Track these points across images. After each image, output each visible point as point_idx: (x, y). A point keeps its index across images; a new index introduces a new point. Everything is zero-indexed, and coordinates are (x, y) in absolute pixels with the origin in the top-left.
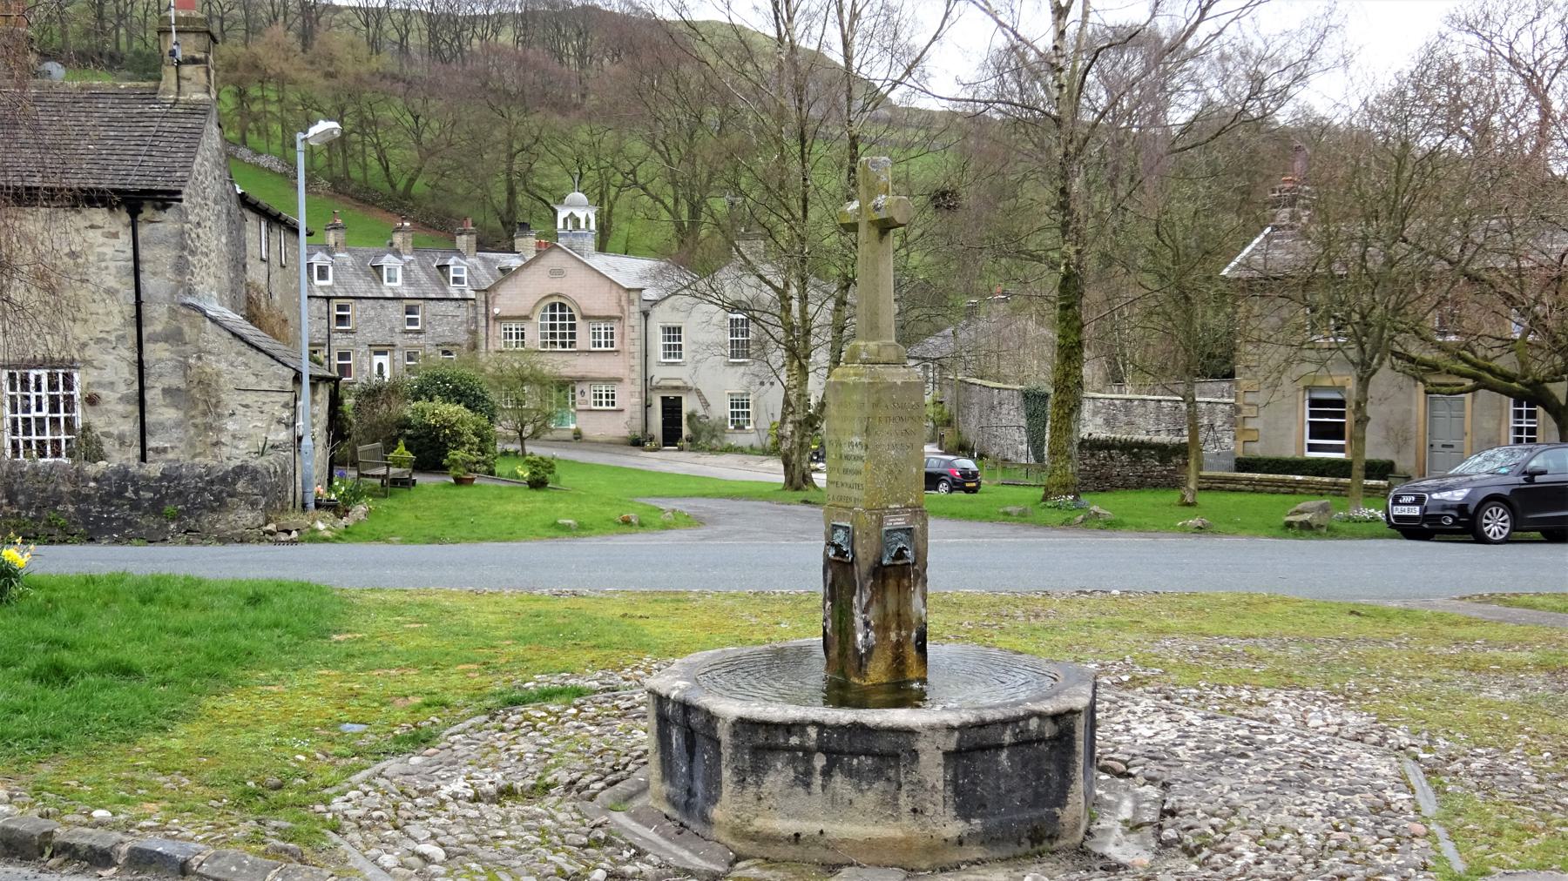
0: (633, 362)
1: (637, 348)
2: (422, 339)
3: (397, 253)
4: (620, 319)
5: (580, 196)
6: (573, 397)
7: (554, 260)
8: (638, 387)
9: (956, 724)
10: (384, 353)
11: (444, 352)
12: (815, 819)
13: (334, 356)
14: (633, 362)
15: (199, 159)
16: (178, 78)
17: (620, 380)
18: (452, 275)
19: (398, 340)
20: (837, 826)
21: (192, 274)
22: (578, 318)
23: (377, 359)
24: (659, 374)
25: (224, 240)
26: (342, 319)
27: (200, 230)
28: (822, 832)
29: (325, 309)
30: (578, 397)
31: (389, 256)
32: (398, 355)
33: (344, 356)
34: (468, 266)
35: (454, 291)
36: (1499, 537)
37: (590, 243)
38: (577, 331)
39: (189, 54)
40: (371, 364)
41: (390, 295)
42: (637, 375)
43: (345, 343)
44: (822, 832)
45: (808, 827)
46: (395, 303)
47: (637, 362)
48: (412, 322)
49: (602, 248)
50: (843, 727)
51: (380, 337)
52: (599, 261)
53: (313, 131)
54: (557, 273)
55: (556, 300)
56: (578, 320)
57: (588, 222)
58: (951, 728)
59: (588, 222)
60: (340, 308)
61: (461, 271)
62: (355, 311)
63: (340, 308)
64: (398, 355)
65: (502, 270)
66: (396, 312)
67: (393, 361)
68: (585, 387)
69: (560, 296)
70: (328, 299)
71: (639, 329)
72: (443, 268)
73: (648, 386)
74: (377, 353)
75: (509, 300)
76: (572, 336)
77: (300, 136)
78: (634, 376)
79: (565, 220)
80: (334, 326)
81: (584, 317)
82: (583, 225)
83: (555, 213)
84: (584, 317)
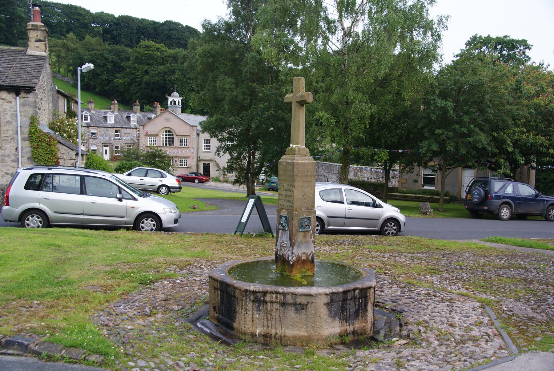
7: (167, 115)
8: (195, 160)
10: (107, 146)
15: (42, 76)
17: (189, 157)
23: (105, 148)
25: (51, 105)
30: (174, 162)
37: (179, 110)
38: (175, 140)
42: (195, 155)
46: (111, 129)
48: (118, 136)
49: (183, 111)
55: (168, 129)
57: (179, 102)
58: (327, 294)
59: (179, 102)
66: (112, 132)
69: (169, 128)
73: (199, 161)
74: (105, 146)
76: (173, 141)
77: (79, 68)
78: (193, 155)
81: (177, 135)
82: (177, 103)
84: (177, 135)
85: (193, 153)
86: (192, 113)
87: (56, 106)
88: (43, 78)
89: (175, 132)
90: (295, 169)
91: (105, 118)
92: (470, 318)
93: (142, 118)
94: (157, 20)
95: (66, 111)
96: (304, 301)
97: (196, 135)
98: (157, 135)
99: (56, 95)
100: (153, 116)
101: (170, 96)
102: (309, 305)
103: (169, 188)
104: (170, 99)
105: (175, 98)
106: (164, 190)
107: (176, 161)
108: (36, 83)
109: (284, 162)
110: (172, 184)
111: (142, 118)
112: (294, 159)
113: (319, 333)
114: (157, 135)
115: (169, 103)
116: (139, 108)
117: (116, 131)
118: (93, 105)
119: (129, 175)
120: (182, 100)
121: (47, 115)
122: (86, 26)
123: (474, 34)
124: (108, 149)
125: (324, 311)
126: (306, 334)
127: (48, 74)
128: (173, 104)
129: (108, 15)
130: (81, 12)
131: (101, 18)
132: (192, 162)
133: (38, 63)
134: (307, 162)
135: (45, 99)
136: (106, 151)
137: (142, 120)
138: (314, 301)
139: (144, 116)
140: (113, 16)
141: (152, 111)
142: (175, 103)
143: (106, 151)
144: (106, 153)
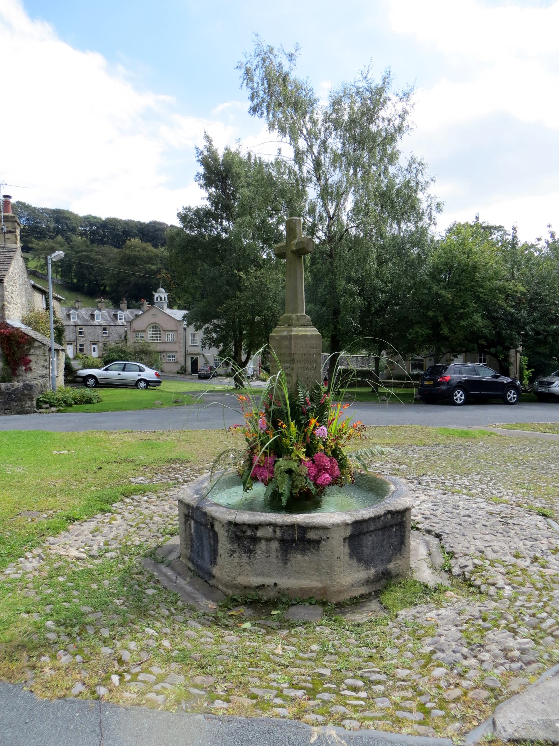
0: (181, 345)
1: (182, 341)
2: (109, 339)
3: (100, 310)
4: (176, 331)
5: (163, 290)
6: (161, 358)
7: (153, 311)
8: (183, 354)
9: (349, 522)
10: (95, 344)
11: (117, 343)
12: (270, 576)
13: (78, 345)
14: (181, 345)
15: (12, 269)
16: (5, 238)
17: (176, 352)
18: (119, 317)
19: (100, 339)
20: (284, 581)
21: (9, 311)
22: (162, 331)
23: (93, 346)
24: (190, 350)
25: (24, 299)
26: (80, 333)
27: (12, 295)
28: (275, 584)
29: (74, 329)
30: (162, 357)
31: (97, 311)
32: (100, 345)
33: (81, 345)
34: (125, 314)
35: (120, 323)
36: (513, 401)
37: (165, 305)
38: (162, 336)
39: (9, 229)
40: (91, 348)
41: (98, 324)
42: (182, 350)
43: (82, 340)
44: (275, 584)
45: (268, 581)
46: (99, 327)
47: (182, 345)
48: (106, 333)
49: (170, 307)
50: (287, 526)
51: (94, 338)
52: (169, 312)
53: (53, 255)
54: (154, 316)
55: (154, 325)
56: (162, 332)
57: (165, 298)
58: (347, 525)
59: (165, 298)
60: (80, 329)
61: (122, 316)
62: (85, 330)
63: (80, 329)
64: (100, 345)
65: (136, 315)
66: (99, 330)
67: (99, 347)
68: (164, 354)
69: (155, 323)
70: (76, 326)
71: (182, 336)
72: (115, 315)
73: (186, 354)
74: (93, 344)
75: (137, 325)
76: (160, 337)
77: (49, 257)
78: (181, 350)
79: (157, 298)
80: (78, 335)
81: (164, 331)
82: (163, 299)
83: (153, 295)
84: (164, 331)
85: (180, 347)
86: (179, 308)
87: (30, 302)
88: (14, 271)
89: (162, 327)
90: (293, 344)
91: (92, 316)
92: (538, 542)
93: (129, 315)
94: (142, 221)
95: (44, 307)
96: (314, 536)
97: (182, 330)
98: (144, 331)
99: (31, 289)
100: (141, 312)
101: (156, 292)
102: (323, 542)
103: (147, 382)
104: (156, 295)
105: (161, 294)
106: (142, 385)
107: (164, 356)
108: (4, 275)
109: (277, 336)
110: (150, 378)
111: (129, 315)
112: (291, 331)
113: (338, 583)
114: (144, 331)
115: (155, 299)
116: (126, 305)
117: (104, 329)
118: (80, 304)
119: (106, 370)
120: (168, 296)
121: (19, 310)
122: (74, 230)
123: (454, 221)
124: (96, 346)
125: (344, 550)
126: (319, 585)
127: (20, 267)
128: (159, 300)
129: (95, 218)
130: (67, 215)
131: (89, 221)
132: (180, 357)
133: (8, 255)
134: (309, 334)
135: (17, 293)
136: (94, 348)
137: (129, 317)
138: (329, 536)
139: (131, 313)
140: (100, 219)
141: (139, 308)
142: (161, 298)
143: (94, 348)
144: (94, 351)
